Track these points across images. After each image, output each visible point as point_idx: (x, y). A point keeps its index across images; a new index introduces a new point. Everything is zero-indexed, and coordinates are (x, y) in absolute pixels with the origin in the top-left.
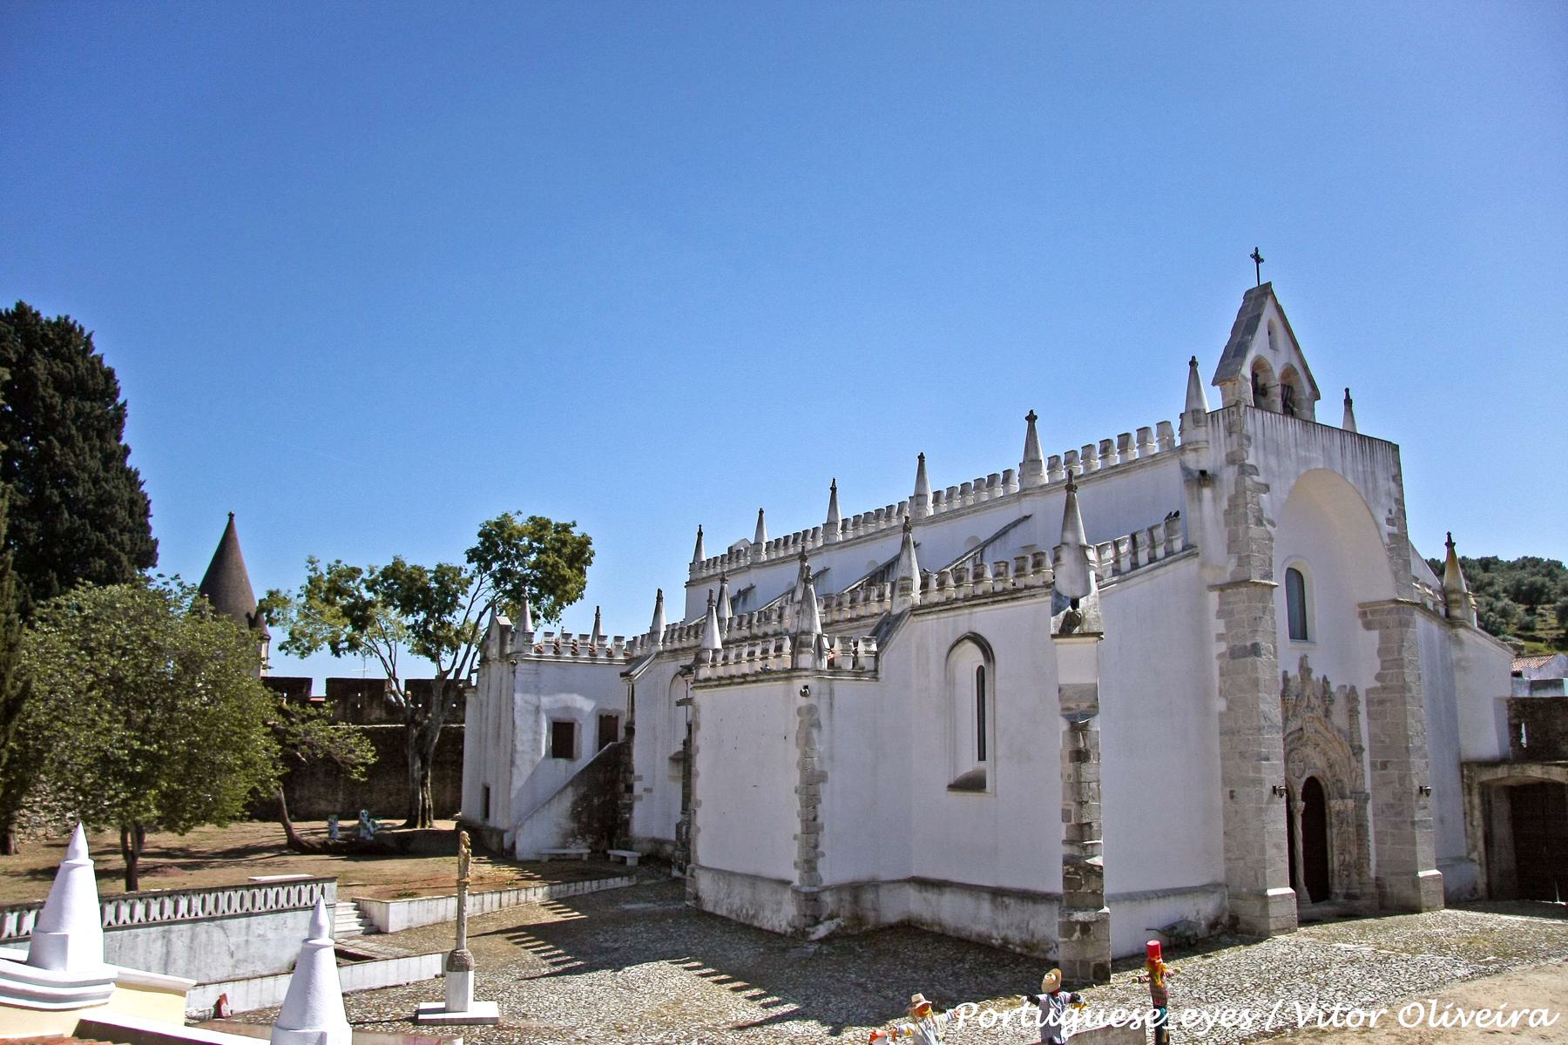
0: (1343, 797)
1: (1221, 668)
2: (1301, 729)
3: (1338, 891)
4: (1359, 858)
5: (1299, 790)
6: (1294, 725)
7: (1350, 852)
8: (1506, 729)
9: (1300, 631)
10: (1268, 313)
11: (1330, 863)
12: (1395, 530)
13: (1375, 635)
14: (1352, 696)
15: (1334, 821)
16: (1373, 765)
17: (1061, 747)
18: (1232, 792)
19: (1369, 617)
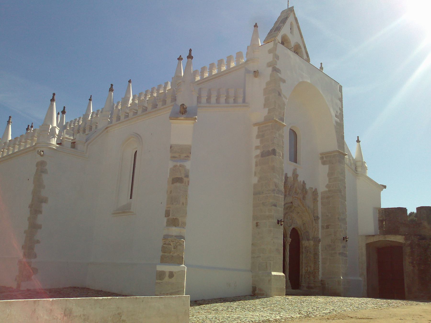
0: (308, 240)
1: (256, 162)
2: (292, 203)
3: (304, 285)
4: (314, 269)
5: (289, 233)
6: (289, 199)
7: (310, 267)
8: (377, 222)
9: (294, 158)
10: (291, 19)
11: (301, 271)
12: (338, 120)
13: (327, 167)
14: (315, 193)
15: (304, 250)
16: (323, 227)
17: (168, 177)
18: (257, 223)
19: (325, 159)
